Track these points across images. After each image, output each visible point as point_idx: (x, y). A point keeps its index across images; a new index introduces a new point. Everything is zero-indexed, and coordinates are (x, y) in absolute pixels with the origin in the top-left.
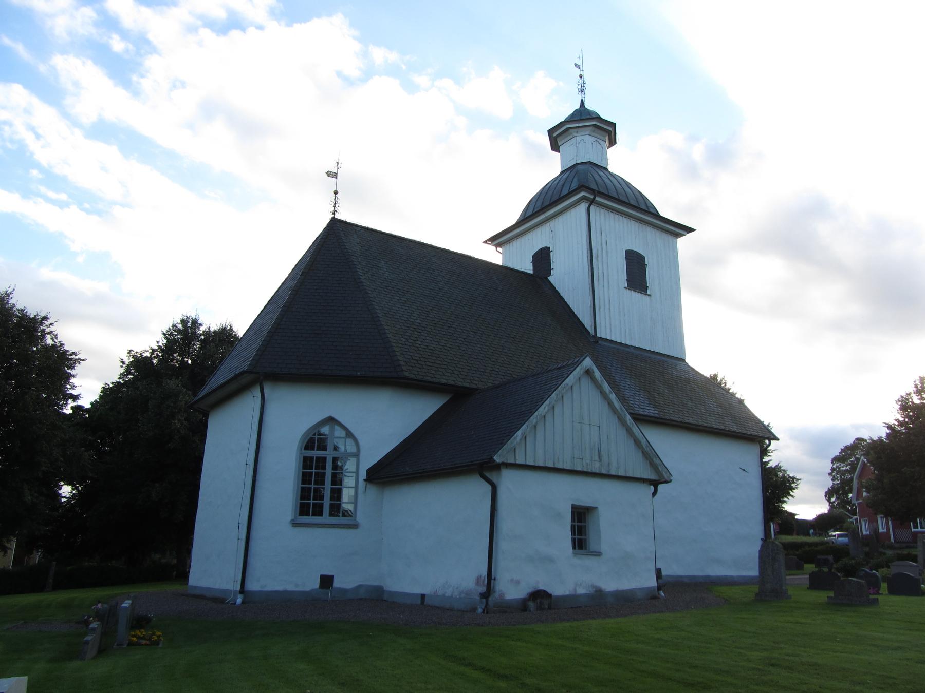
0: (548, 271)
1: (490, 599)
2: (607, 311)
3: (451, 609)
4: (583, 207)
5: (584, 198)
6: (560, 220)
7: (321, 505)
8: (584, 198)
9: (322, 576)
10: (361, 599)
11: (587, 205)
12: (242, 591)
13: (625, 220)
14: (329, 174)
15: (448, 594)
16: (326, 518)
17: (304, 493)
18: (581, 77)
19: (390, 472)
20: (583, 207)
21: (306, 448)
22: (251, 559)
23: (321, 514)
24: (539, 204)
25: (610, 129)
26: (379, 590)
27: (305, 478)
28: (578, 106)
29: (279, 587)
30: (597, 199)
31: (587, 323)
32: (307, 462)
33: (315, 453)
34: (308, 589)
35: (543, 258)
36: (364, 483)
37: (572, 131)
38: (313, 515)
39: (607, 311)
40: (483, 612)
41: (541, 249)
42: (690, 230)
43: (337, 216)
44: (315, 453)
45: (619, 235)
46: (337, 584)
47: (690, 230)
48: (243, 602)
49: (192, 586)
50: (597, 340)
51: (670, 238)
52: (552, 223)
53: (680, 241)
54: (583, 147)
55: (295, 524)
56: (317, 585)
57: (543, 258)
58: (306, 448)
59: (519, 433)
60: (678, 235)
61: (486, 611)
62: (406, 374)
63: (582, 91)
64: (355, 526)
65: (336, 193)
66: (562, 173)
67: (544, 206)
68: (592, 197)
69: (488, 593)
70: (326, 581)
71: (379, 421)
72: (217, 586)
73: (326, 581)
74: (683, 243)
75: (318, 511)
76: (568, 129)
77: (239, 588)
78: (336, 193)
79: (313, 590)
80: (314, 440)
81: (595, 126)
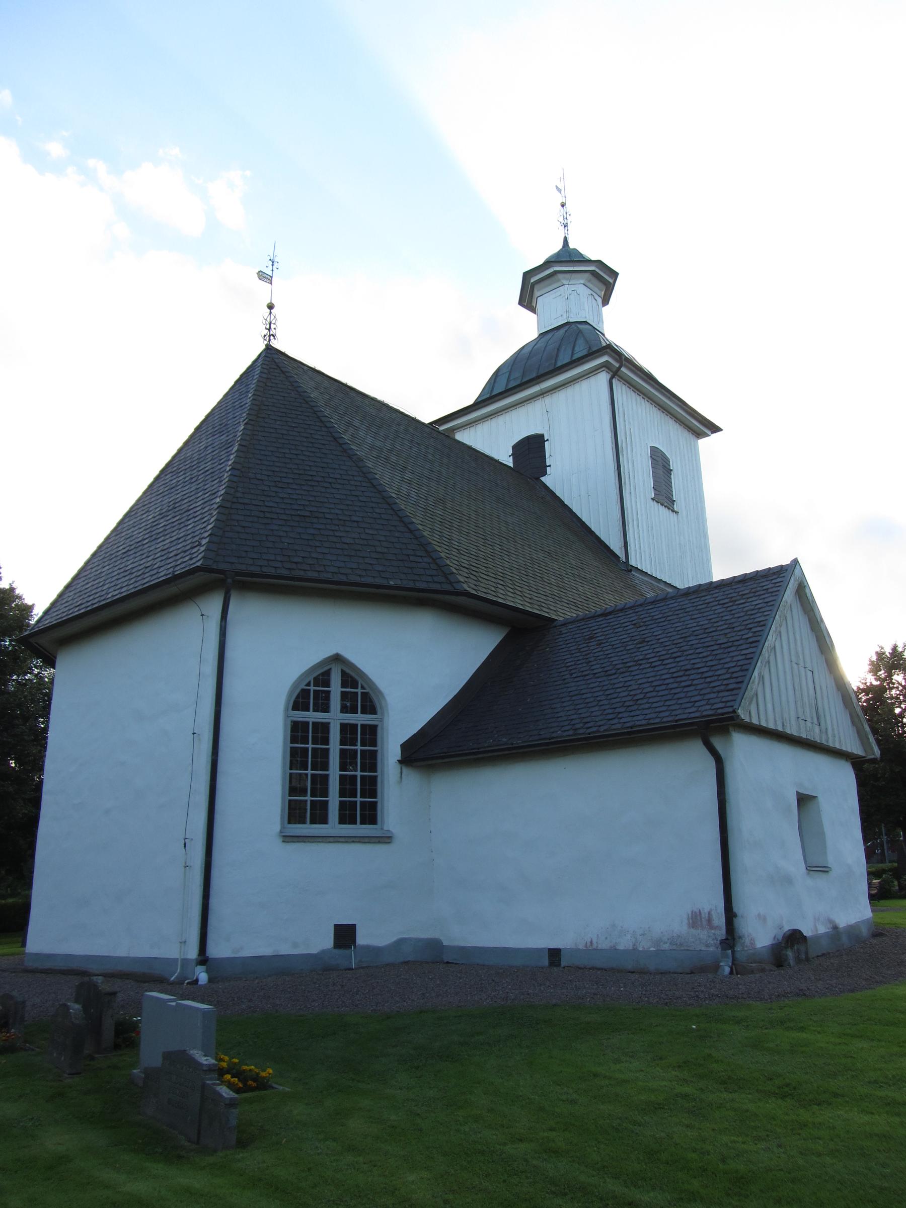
0: (542, 469)
1: (738, 948)
2: (636, 527)
3: (643, 972)
4: (603, 378)
5: (606, 366)
6: (561, 397)
7: (325, 805)
8: (606, 366)
9: (336, 926)
10: (407, 963)
11: (609, 376)
12: (203, 959)
13: (648, 404)
14: (262, 276)
15: (625, 943)
16: (334, 826)
17: (294, 788)
18: (563, 205)
19: (444, 746)
20: (603, 378)
21: (296, 707)
22: (213, 902)
23: (324, 820)
24: (517, 374)
25: (611, 281)
26: (435, 945)
27: (296, 758)
28: (558, 246)
29: (265, 950)
30: (623, 369)
31: (615, 545)
32: (297, 731)
33: (312, 716)
34: (314, 951)
35: (532, 450)
36: (398, 766)
37: (560, 276)
38: (313, 822)
39: (636, 527)
40: (731, 973)
41: (528, 438)
42: (715, 429)
43: (275, 344)
44: (312, 716)
45: (646, 428)
46: (362, 939)
47: (715, 429)
48: (210, 980)
49: (369, 949)
50: (630, 569)
51: (692, 437)
52: (548, 400)
53: (702, 443)
54: (567, 303)
55: (287, 839)
56: (328, 942)
57: (532, 450)
58: (296, 707)
59: (756, 673)
60: (699, 435)
61: (736, 968)
62: (465, 586)
63: (566, 226)
64: (386, 839)
65: (271, 307)
66: (542, 335)
67: (520, 378)
68: (617, 365)
69: (731, 936)
70: (345, 935)
71: (418, 666)
72: (247, 953)
73: (345, 935)
74: (706, 445)
75: (320, 816)
76: (556, 272)
77: (193, 953)
78: (271, 307)
79: (323, 952)
80: (309, 694)
81: (593, 273)
